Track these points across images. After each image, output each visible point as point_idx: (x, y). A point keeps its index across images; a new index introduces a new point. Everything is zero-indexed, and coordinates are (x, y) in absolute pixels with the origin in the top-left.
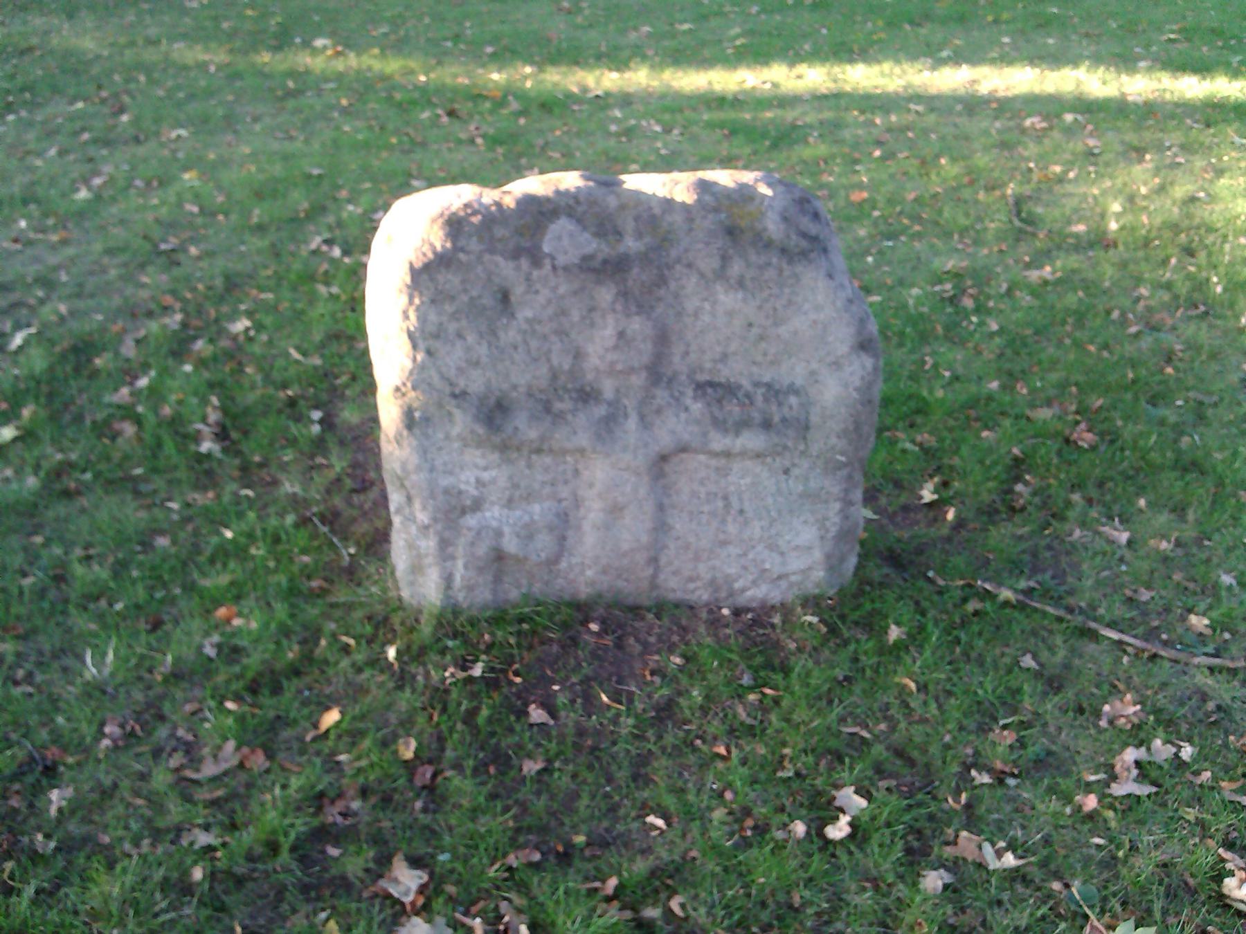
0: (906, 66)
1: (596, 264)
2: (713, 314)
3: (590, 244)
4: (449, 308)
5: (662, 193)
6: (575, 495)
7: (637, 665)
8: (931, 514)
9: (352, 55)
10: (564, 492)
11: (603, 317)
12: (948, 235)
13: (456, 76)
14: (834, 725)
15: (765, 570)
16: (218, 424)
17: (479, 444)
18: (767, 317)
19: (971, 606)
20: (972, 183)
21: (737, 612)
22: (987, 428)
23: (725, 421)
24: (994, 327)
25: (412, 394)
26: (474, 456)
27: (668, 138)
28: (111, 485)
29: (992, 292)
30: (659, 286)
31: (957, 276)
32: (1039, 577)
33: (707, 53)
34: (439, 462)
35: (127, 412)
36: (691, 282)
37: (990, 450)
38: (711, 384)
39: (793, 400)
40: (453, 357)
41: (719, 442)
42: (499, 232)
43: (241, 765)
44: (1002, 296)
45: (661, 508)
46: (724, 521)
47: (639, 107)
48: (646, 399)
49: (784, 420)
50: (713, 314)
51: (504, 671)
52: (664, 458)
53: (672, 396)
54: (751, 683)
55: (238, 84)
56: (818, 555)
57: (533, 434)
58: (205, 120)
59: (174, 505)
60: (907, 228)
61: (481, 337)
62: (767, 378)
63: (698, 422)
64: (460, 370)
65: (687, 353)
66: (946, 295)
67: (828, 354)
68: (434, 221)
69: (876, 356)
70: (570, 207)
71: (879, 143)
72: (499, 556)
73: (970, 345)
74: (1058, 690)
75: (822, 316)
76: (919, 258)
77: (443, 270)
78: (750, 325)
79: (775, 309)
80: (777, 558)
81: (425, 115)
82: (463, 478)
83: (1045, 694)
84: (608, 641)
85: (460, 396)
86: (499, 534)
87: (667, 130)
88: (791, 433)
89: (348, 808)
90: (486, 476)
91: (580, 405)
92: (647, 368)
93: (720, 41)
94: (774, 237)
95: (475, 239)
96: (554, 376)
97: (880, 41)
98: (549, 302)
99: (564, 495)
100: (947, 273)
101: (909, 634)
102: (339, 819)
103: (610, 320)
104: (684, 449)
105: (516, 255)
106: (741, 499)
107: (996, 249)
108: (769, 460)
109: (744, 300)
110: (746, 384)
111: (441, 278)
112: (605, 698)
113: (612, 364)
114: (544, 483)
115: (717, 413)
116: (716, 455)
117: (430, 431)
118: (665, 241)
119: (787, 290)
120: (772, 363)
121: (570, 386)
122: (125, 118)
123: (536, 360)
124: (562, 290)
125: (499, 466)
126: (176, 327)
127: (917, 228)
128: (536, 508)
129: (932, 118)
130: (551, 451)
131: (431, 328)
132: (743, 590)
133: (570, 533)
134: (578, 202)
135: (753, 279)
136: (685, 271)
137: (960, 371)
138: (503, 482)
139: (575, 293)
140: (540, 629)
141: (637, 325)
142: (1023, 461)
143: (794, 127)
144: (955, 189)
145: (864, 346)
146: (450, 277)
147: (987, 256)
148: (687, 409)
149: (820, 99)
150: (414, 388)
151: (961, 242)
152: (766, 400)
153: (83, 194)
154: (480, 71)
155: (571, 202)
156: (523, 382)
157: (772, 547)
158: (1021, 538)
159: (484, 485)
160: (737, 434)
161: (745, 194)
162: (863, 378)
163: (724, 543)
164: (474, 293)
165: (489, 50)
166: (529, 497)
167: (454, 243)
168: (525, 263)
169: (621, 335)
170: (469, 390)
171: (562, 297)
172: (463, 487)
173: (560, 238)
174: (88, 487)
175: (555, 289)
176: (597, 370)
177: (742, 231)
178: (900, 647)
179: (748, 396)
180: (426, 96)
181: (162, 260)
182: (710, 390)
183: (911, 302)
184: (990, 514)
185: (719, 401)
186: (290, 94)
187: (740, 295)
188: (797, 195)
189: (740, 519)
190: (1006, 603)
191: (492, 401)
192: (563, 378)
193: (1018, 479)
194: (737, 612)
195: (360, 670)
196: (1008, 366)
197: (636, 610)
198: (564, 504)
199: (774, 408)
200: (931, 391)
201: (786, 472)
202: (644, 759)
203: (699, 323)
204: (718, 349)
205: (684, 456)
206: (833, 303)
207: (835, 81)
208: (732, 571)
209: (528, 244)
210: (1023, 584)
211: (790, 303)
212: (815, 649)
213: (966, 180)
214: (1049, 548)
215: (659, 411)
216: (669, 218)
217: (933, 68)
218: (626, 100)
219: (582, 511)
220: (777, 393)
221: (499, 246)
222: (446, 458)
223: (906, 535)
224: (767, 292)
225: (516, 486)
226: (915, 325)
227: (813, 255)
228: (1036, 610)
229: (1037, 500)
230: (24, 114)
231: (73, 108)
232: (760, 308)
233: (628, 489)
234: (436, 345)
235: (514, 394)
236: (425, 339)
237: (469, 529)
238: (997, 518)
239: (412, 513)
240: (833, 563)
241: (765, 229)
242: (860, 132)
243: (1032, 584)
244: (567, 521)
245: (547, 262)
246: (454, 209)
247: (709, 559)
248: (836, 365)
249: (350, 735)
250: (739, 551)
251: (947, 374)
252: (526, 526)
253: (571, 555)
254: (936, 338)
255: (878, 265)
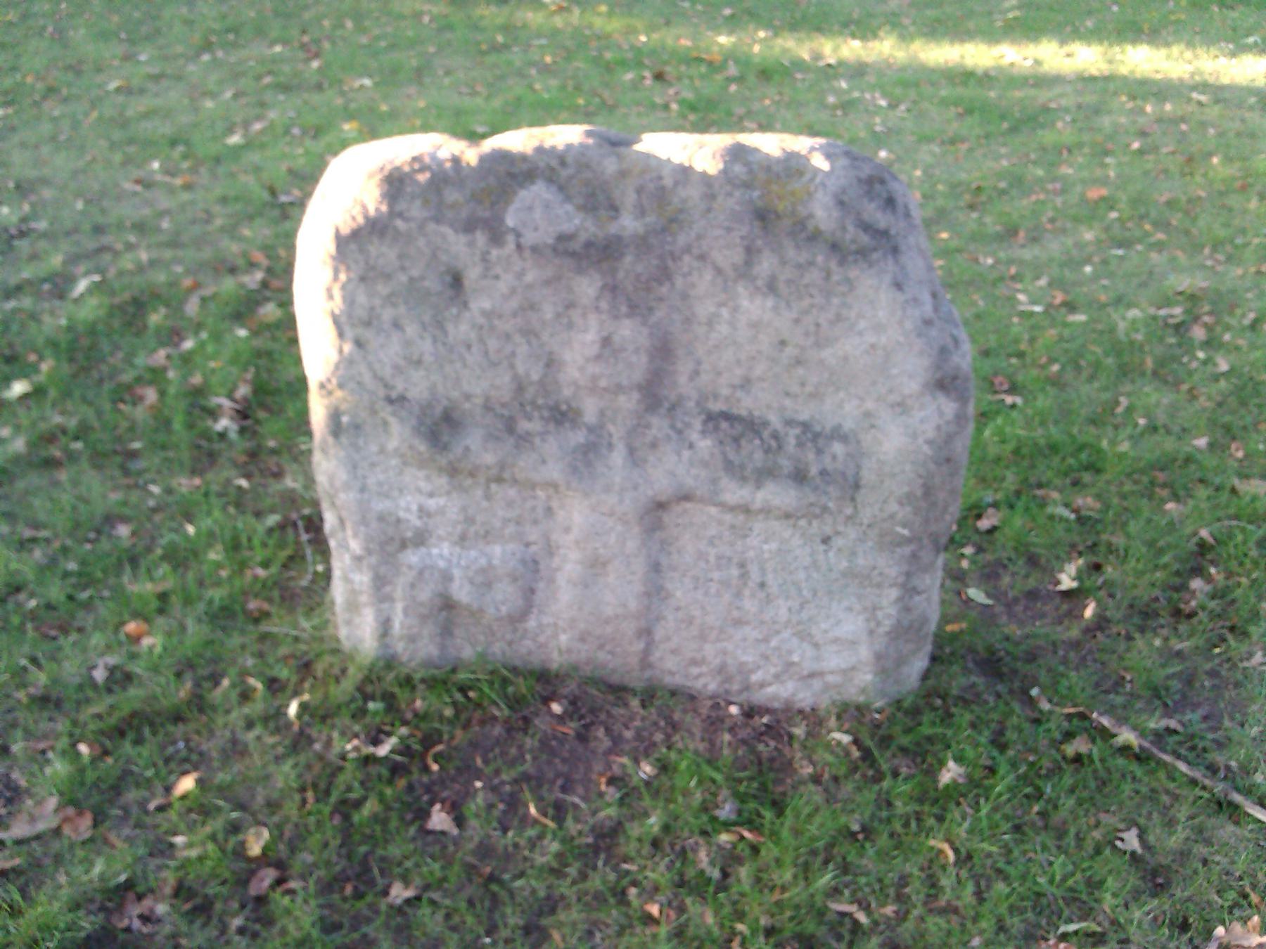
0: (1201, 51)
1: (576, 246)
2: (732, 324)
3: (571, 219)
4: (383, 289)
5: (679, 158)
6: (547, 539)
7: (598, 767)
8: (1065, 607)
9: (577, 11)
10: (533, 534)
11: (584, 315)
12: (1197, 248)
13: (678, 38)
14: (819, 900)
15: (792, 664)
16: (245, 399)
17: (422, 464)
18: (807, 334)
19: (1079, 745)
20: (1244, 188)
21: (750, 712)
22: (1176, 497)
23: (742, 467)
24: (1224, 367)
25: (339, 394)
26: (416, 478)
27: (891, 114)
28: (98, 459)
29: (1233, 322)
30: (661, 283)
31: (1193, 299)
32: (1189, 716)
33: (971, 25)
34: (371, 481)
35: (156, 376)
36: (704, 281)
37: (1172, 526)
38: (726, 416)
39: (838, 448)
40: (389, 351)
41: (734, 493)
42: (452, 195)
43: (57, 832)
44: (1243, 329)
45: (656, 568)
46: (738, 595)
47: (871, 79)
48: (639, 427)
49: (823, 473)
50: (732, 324)
51: (423, 756)
52: (661, 506)
53: (673, 427)
54: (733, 817)
55: (448, 35)
56: (865, 653)
57: (489, 458)
58: (394, 71)
59: (155, 489)
60: (1147, 234)
61: (424, 327)
62: (804, 416)
63: (705, 464)
64: (397, 369)
65: (696, 373)
66: (1171, 321)
67: (891, 391)
68: (371, 176)
69: (963, 399)
70: (553, 170)
71: (1143, 134)
72: (448, 605)
73: (1185, 387)
74: (1159, 889)
75: (883, 340)
76: (1151, 273)
77: (375, 240)
78: (783, 343)
79: (818, 325)
80: (810, 652)
81: (629, 76)
82: (402, 503)
83: (1136, 895)
84: (571, 728)
85: (397, 401)
86: (447, 577)
87: (893, 106)
88: (832, 490)
89: (152, 910)
90: (432, 503)
91: (551, 427)
92: (640, 388)
93: (990, 13)
94: (823, 227)
95: (418, 203)
96: (520, 388)
97: (1177, 22)
98: (513, 291)
99: (532, 538)
100: (1181, 293)
101: (970, 778)
102: (137, 924)
103: (593, 320)
104: (687, 498)
105: (469, 227)
106: (763, 571)
107: (1253, 270)
108: (803, 522)
109: (775, 309)
110: (775, 420)
111: (373, 249)
112: (533, 810)
113: (594, 378)
114: (506, 521)
115: (732, 455)
116: (732, 509)
117: (361, 442)
118: (673, 222)
119: (835, 301)
120: (812, 396)
121: (540, 401)
122: (315, 64)
123: (494, 365)
124: (530, 277)
125: (448, 493)
126: (253, 286)
127: (1160, 236)
128: (497, 550)
129: (1216, 110)
130: (515, 481)
131: (361, 313)
132: (762, 685)
133: (541, 585)
134: (563, 163)
135: (789, 282)
136: (696, 264)
137: (1161, 418)
138: (453, 513)
139: (548, 282)
140: (486, 703)
141: (627, 330)
142: (1212, 548)
143: (1046, 109)
144: (1222, 194)
145: (945, 383)
146: (384, 249)
147: (1242, 277)
148: (691, 446)
149: (1086, 81)
150: (341, 386)
151: (1211, 257)
152: (800, 444)
153: (235, 139)
154: (710, 33)
155: (554, 163)
156: (478, 391)
157: (804, 636)
158: (1179, 654)
159: (429, 515)
160: (759, 485)
161: (793, 166)
162: (938, 428)
163: (738, 623)
164: (415, 273)
165: (727, 12)
166: (487, 536)
167: (391, 206)
168: (481, 238)
169: (606, 341)
170: (409, 395)
171: (530, 286)
172: (402, 514)
173: (530, 209)
174: (72, 457)
175: (520, 275)
176: (575, 383)
177: (778, 217)
178: (954, 794)
179: (775, 436)
180: (637, 59)
181: (276, 213)
182: (724, 425)
183: (1122, 326)
184: (1145, 616)
185: (736, 440)
186: (496, 48)
187: (770, 303)
188: (866, 171)
189: (762, 595)
190: (1125, 750)
191: (438, 411)
192: (530, 393)
193: (1198, 571)
194: (750, 712)
195: (250, 725)
196: (1227, 419)
197: (619, 691)
198: (534, 548)
199: (811, 456)
200: (1113, 443)
201: (826, 540)
202: (552, 905)
203: (714, 335)
204: (739, 372)
205: (688, 505)
206: (900, 323)
207: (1110, 62)
208: (749, 658)
209: (487, 214)
210: (1155, 723)
211: (839, 318)
212: (836, 779)
213: (1238, 184)
214: (1213, 674)
215: (654, 445)
216: (682, 193)
217: (1233, 55)
218: (858, 71)
219: (556, 561)
220: (817, 436)
221: (450, 214)
222: (381, 477)
223: (1015, 631)
224: (806, 302)
225: (470, 520)
226: (1119, 354)
227: (875, 256)
228: (1160, 763)
229: (1212, 604)
230: (220, 54)
231: (269, 52)
232: (797, 321)
233: (612, 539)
234: (368, 334)
235: (467, 406)
236: (353, 325)
237: (410, 567)
238: (1152, 623)
239: (345, 539)
240: (886, 665)
241: (811, 216)
242: (1123, 120)
243: (1173, 724)
244: (537, 571)
245: (510, 239)
246: (398, 163)
247: (718, 640)
248: (901, 407)
249: (199, 808)
250: (756, 634)
251: (1142, 421)
252: (483, 571)
253: (541, 612)
254: (1143, 374)
255: (1095, 277)
